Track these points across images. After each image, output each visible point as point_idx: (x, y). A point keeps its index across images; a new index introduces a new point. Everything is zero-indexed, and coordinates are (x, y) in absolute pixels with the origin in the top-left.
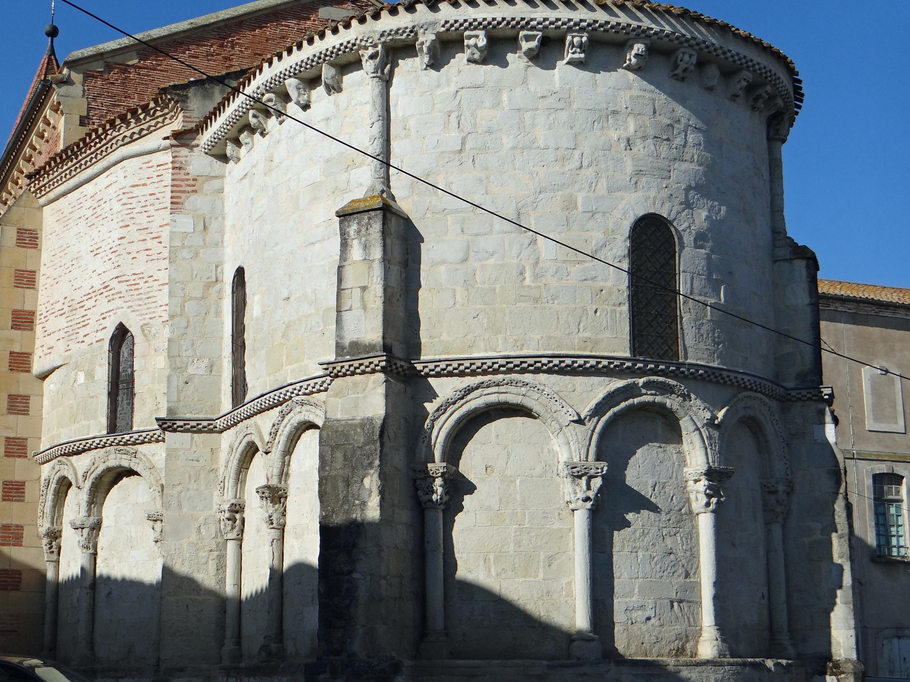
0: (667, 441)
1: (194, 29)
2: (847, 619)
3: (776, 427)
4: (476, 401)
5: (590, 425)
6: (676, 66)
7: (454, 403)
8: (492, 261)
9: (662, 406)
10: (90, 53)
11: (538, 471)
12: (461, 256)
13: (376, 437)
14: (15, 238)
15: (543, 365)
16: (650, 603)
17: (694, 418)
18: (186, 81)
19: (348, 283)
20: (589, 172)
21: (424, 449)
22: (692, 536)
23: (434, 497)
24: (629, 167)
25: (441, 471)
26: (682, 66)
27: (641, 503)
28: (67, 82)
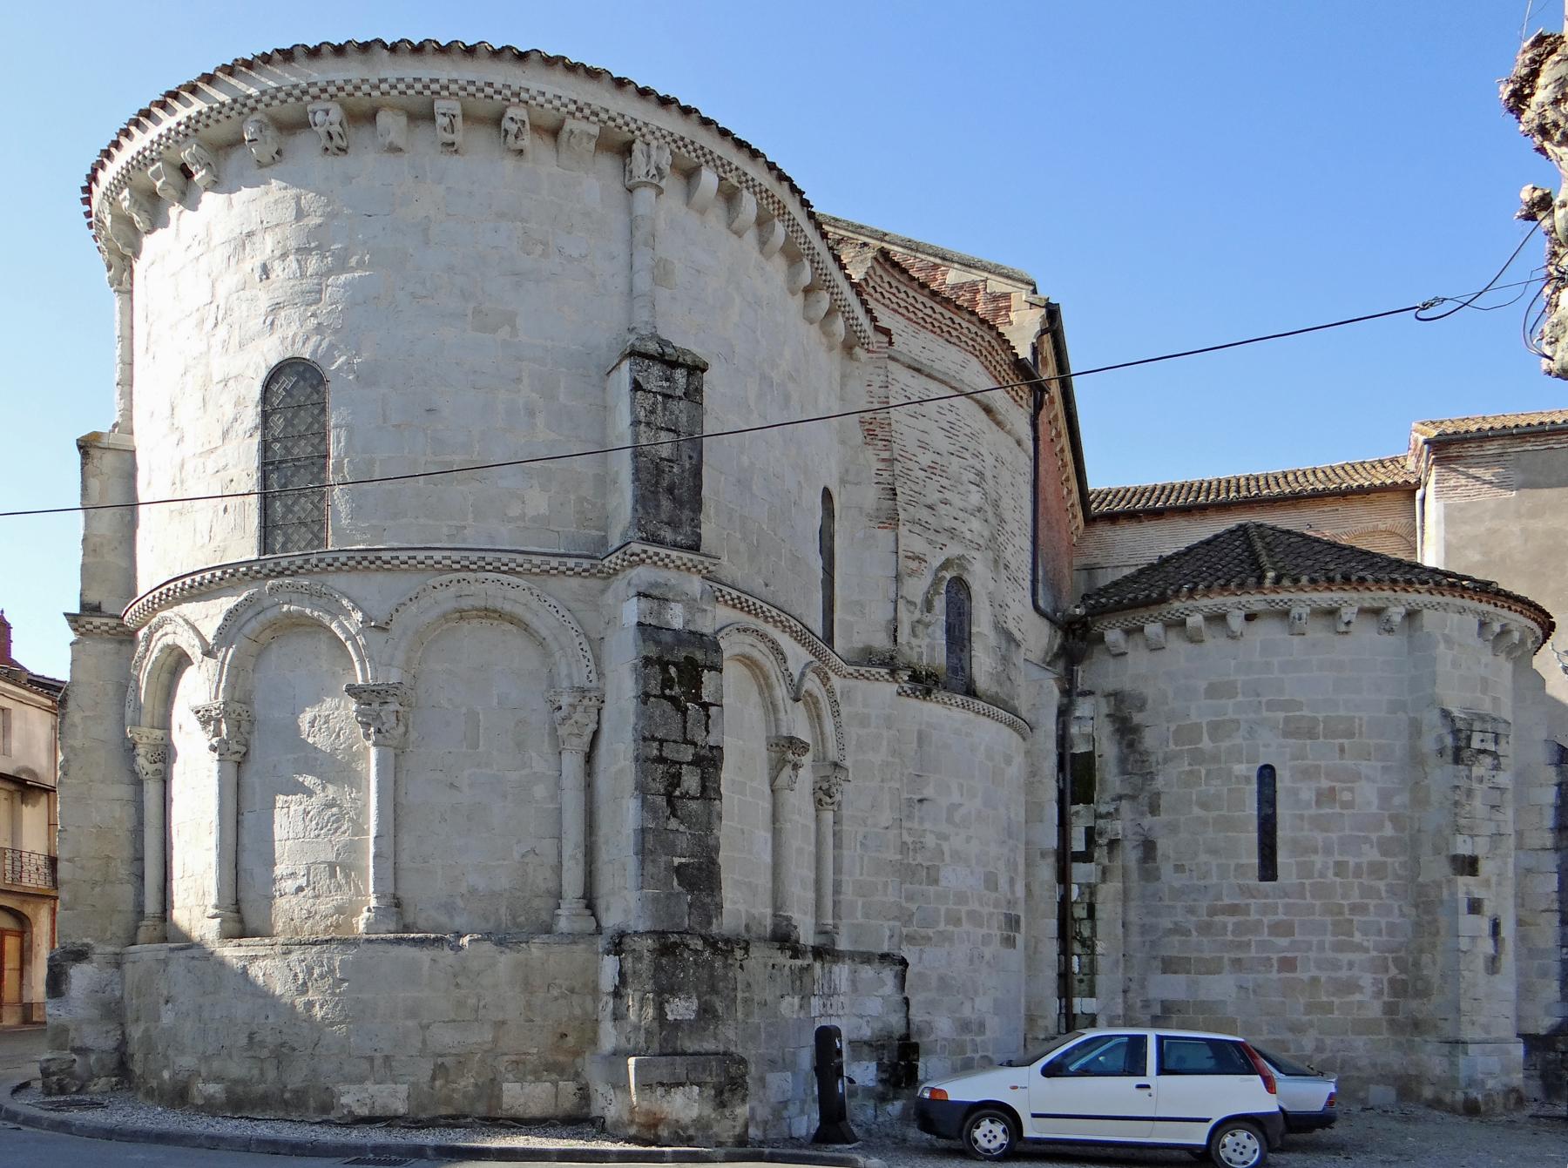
24: (264, 303)
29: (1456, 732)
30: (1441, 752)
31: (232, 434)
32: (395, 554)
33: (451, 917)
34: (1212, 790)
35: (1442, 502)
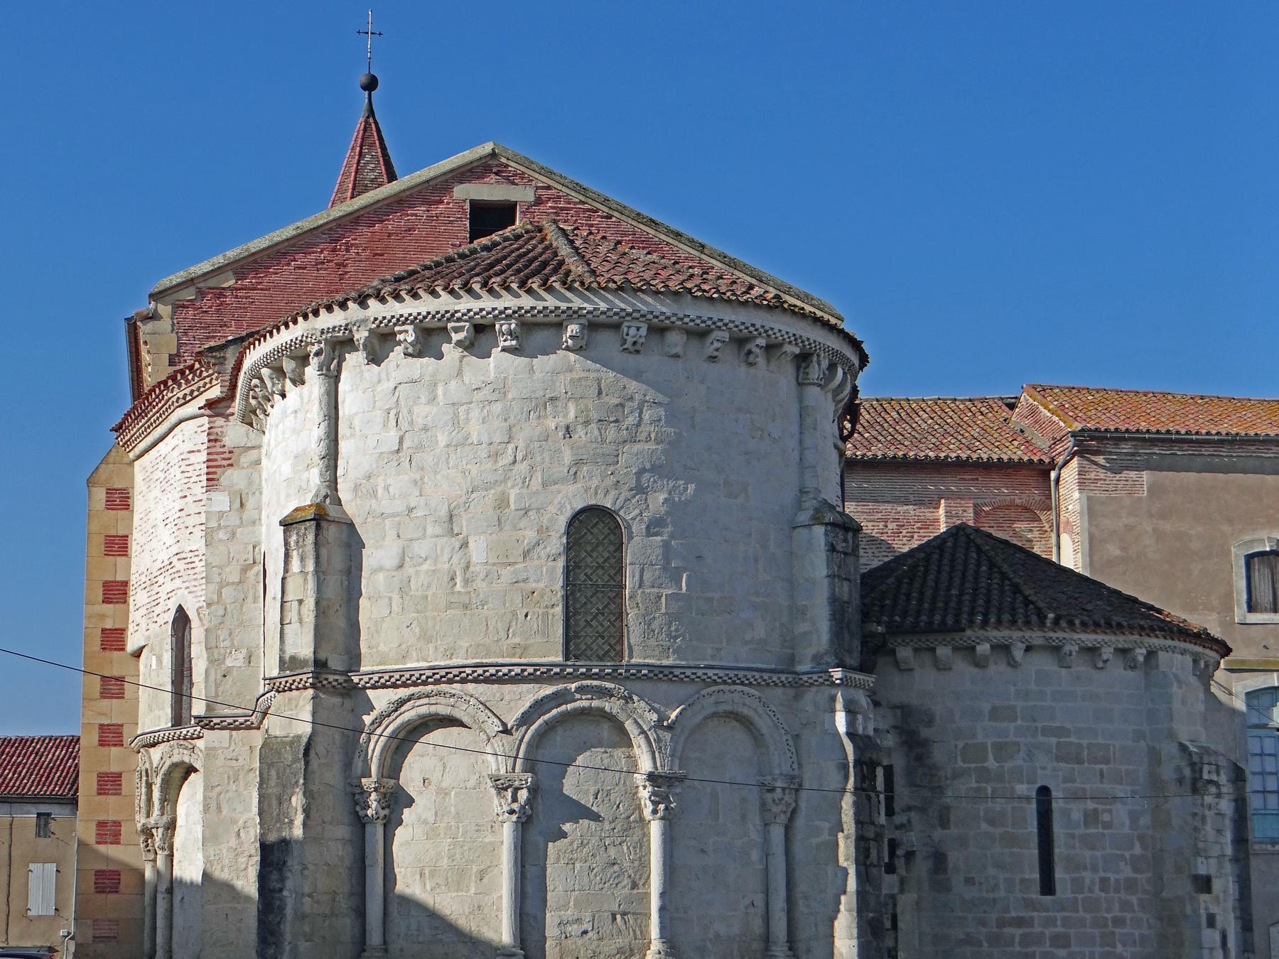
1: (300, 235)
2: (850, 928)
4: (409, 713)
5: (517, 735)
6: (625, 341)
8: (425, 567)
9: (602, 710)
10: (179, 280)
11: (471, 783)
12: (395, 562)
13: (301, 756)
14: (104, 499)
16: (587, 916)
18: (223, 341)
19: (289, 597)
20: (522, 468)
21: (360, 764)
22: (643, 844)
23: (369, 812)
24: (568, 457)
26: (630, 340)
27: (581, 812)
28: (153, 317)
29: (1192, 765)
30: (1180, 781)
31: (534, 554)
34: (998, 807)
35: (1085, 495)
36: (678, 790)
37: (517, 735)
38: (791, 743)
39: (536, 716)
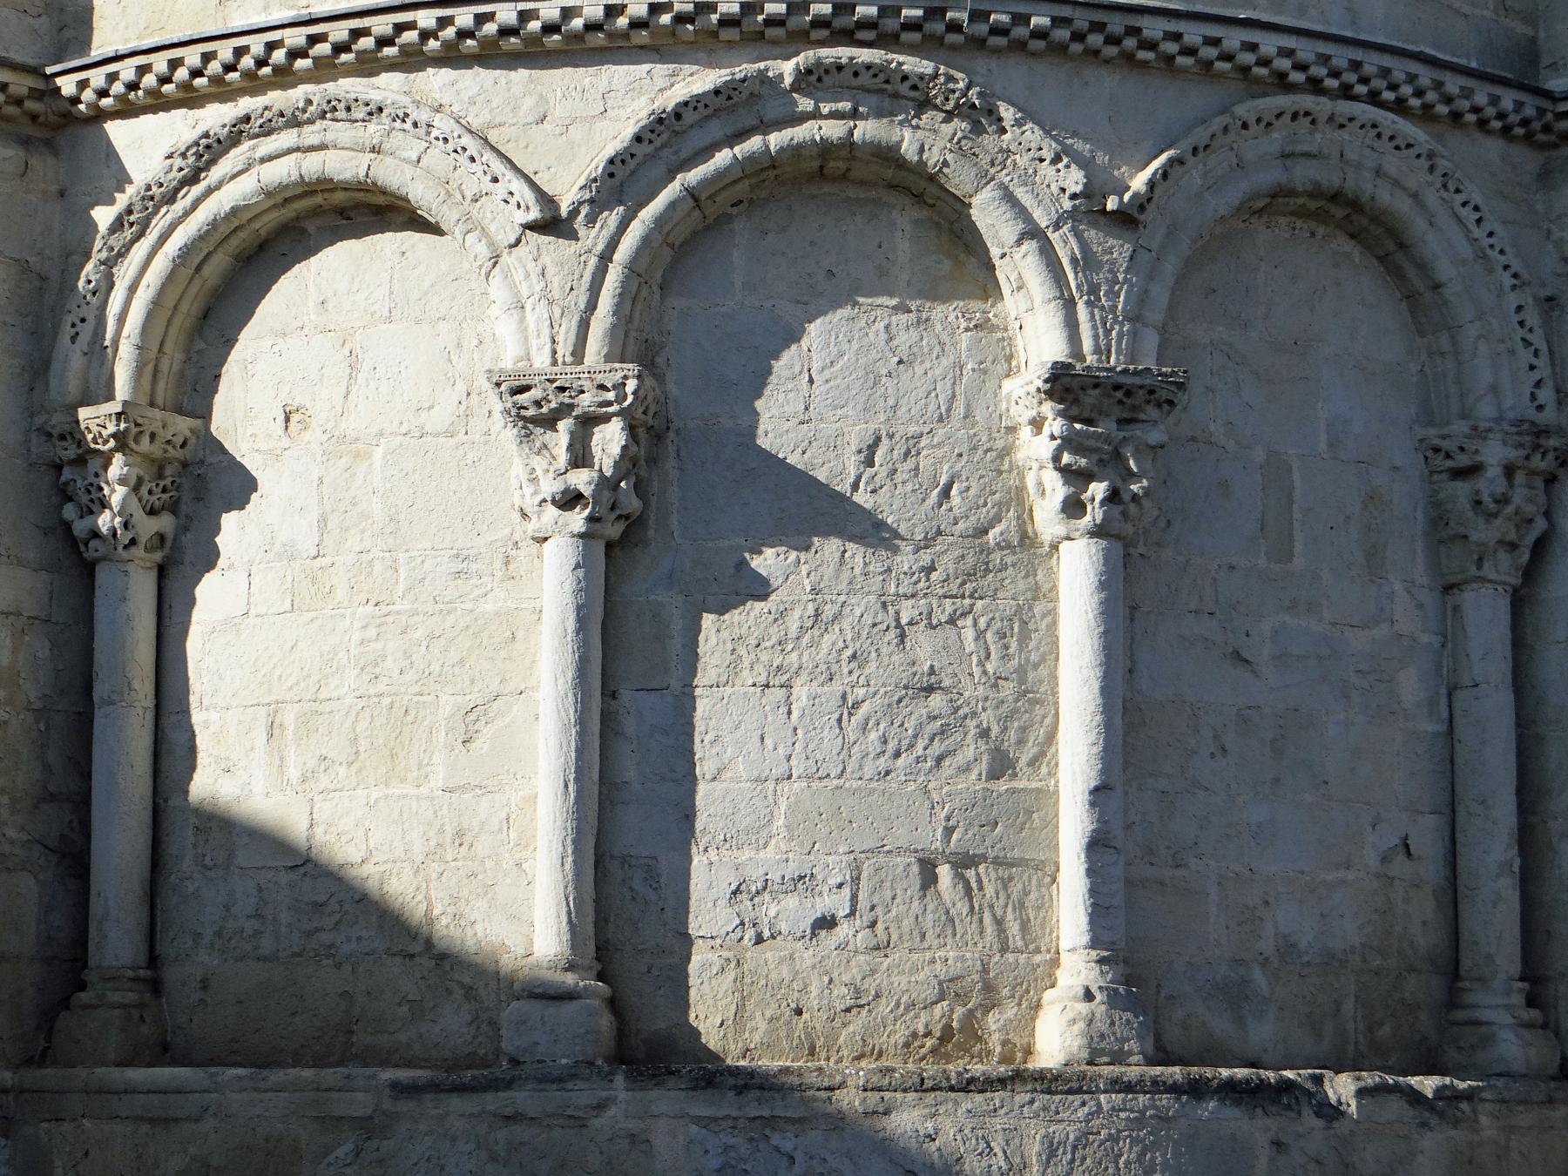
0: (936, 292)
3: (1479, 233)
4: (237, 185)
5: (593, 238)
7: (171, 198)
9: (887, 154)
11: (439, 417)
15: (426, 35)
17: (1021, 193)
21: (77, 362)
22: (1028, 625)
23: (105, 521)
25: (112, 428)
27: (810, 510)
32: (1173, 26)
33: (1240, 1021)
36: (1155, 436)
37: (593, 238)
38: (1533, 318)
39: (659, 169)
